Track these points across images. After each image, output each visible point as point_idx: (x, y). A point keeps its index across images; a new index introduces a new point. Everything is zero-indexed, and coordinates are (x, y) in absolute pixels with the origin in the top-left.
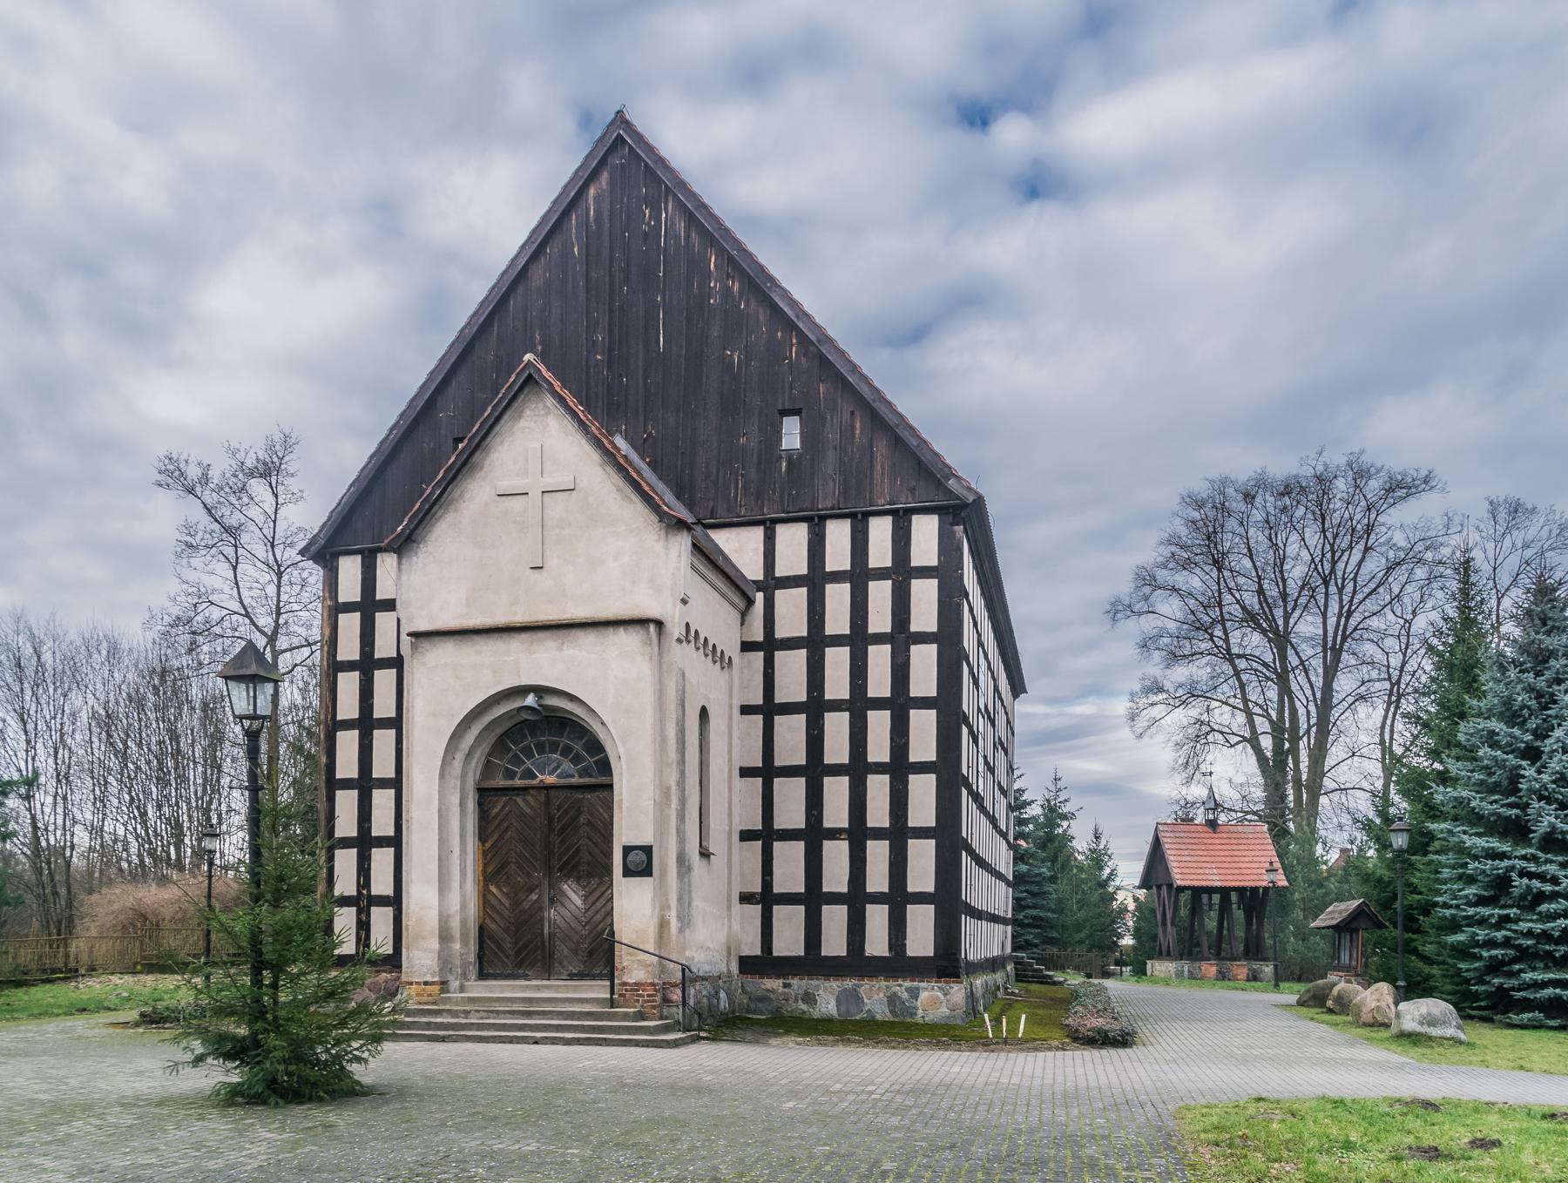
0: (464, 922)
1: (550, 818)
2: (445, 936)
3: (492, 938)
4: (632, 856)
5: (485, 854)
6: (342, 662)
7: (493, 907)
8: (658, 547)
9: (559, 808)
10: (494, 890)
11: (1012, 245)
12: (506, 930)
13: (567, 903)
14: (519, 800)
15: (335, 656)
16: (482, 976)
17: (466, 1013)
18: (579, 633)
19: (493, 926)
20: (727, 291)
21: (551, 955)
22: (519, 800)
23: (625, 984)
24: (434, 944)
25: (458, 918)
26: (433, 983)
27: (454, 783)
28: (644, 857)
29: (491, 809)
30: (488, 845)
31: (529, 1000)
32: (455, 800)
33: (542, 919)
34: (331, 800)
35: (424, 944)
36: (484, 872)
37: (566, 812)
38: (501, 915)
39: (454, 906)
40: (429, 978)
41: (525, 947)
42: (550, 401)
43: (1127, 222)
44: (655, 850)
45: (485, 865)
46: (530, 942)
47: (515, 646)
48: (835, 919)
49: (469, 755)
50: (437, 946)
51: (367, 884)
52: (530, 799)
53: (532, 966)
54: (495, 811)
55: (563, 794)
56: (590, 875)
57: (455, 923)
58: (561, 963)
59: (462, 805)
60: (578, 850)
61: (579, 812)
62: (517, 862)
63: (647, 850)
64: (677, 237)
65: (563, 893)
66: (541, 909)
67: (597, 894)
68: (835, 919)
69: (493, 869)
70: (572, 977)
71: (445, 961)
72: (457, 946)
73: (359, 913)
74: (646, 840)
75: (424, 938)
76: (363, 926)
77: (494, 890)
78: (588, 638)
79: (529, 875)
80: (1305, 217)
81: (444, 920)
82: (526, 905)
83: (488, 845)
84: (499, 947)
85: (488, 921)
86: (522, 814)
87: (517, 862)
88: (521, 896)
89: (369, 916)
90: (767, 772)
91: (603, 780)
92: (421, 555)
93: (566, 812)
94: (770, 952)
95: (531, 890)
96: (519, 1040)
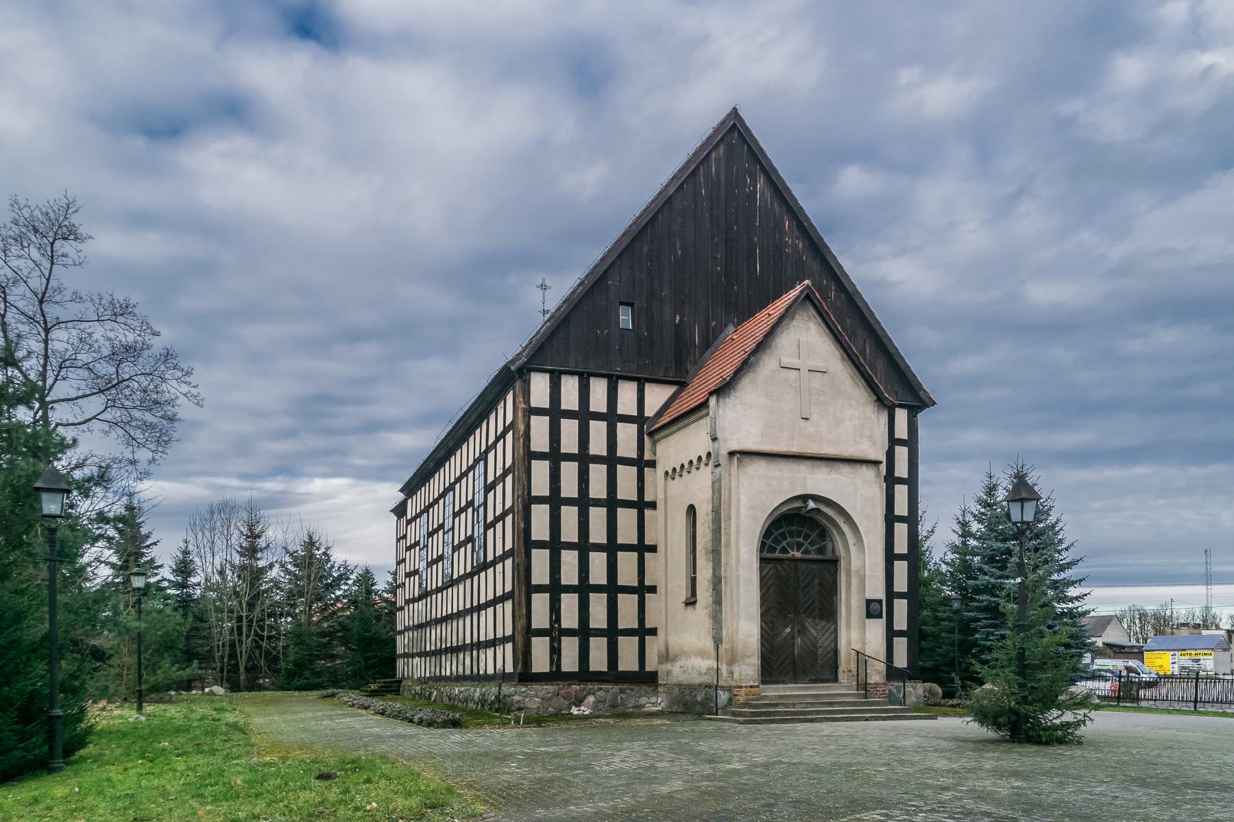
6: (535, 452)
8: (874, 417)
15: (529, 447)
17: (794, 705)
18: (840, 465)
20: (795, 246)
34: (528, 556)
40: (752, 683)
42: (812, 311)
47: (802, 469)
48: (570, 647)
51: (558, 620)
55: (804, 565)
64: (766, 203)
68: (570, 647)
73: (552, 641)
76: (555, 651)
78: (846, 469)
90: (643, 548)
94: (559, 666)
96: (852, 719)
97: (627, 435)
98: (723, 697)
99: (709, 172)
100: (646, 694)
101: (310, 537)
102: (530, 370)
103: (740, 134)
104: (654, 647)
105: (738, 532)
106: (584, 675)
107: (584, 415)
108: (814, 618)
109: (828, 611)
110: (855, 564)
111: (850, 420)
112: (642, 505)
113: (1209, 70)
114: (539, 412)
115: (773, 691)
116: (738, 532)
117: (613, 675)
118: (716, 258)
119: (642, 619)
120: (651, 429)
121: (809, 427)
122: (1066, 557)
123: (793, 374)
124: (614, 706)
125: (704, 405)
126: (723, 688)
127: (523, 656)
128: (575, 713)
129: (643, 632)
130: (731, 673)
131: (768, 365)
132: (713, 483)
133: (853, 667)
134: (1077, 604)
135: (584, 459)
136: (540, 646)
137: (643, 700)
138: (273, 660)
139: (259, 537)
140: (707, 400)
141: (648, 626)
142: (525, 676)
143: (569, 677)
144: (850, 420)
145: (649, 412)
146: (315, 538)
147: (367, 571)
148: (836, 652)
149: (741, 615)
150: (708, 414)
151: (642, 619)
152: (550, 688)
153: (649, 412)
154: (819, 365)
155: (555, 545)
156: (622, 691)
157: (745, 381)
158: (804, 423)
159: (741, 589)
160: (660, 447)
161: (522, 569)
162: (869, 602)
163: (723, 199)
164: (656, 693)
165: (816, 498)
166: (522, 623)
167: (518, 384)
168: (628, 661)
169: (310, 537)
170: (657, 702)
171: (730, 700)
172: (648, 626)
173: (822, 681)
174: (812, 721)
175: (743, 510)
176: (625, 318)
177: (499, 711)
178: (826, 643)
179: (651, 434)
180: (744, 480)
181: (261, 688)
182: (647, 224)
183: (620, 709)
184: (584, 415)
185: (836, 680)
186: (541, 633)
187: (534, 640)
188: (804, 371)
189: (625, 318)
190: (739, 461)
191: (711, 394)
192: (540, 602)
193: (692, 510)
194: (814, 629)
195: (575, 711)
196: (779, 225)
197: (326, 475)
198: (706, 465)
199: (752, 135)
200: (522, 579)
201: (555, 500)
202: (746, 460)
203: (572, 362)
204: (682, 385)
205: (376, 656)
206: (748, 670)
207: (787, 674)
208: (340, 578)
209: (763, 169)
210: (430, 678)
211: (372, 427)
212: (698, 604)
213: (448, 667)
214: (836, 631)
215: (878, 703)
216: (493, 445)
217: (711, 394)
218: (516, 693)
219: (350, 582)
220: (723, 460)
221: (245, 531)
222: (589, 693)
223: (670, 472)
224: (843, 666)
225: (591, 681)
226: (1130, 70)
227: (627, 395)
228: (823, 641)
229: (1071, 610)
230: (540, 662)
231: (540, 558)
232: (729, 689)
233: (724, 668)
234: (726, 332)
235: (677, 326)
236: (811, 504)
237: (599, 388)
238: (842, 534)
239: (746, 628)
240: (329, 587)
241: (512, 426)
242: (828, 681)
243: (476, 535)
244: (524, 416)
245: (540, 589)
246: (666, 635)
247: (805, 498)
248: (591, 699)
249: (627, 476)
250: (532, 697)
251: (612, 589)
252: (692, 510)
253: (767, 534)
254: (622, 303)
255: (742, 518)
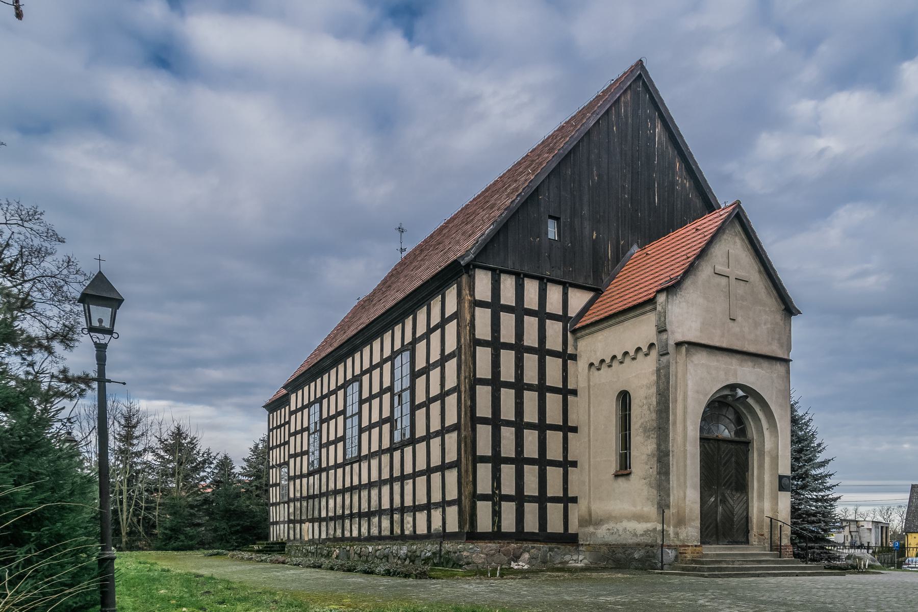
6: (479, 340)
11: (133, 92)
15: (474, 334)
17: (733, 562)
31: (743, 555)
34: (474, 430)
40: (696, 543)
42: (738, 228)
43: (207, 103)
48: (508, 510)
51: (499, 487)
73: (494, 505)
76: (497, 514)
78: (765, 364)
80: (323, 141)
89: (500, 507)
92: (679, 296)
93: (727, 454)
94: (499, 527)
97: (554, 330)
98: (670, 554)
99: (618, 114)
100: (569, 552)
101: (178, 429)
102: (476, 267)
103: (644, 82)
104: (575, 512)
105: (685, 412)
106: (520, 535)
107: (520, 311)
108: (732, 490)
109: (741, 485)
110: (768, 445)
111: (765, 324)
112: (566, 392)
113: (822, 152)
114: (483, 304)
115: (712, 550)
116: (685, 412)
117: (543, 536)
118: (624, 187)
119: (565, 490)
120: (575, 327)
121: (735, 328)
122: (820, 458)
123: (724, 281)
124: (544, 562)
125: (651, 301)
126: (669, 547)
127: (468, 517)
128: (516, 567)
129: (567, 500)
130: (677, 534)
131: (705, 271)
132: (658, 370)
133: (766, 531)
134: (827, 492)
135: (519, 349)
136: (484, 510)
137: (567, 558)
138: (150, 526)
139: (135, 427)
140: (655, 297)
141: (570, 495)
142: (473, 536)
143: (507, 536)
144: (765, 324)
145: (572, 313)
146: (184, 430)
147: (226, 458)
148: (747, 519)
149: (688, 484)
150: (655, 309)
151: (565, 490)
152: (492, 546)
153: (572, 313)
154: (742, 274)
155: (496, 422)
156: (551, 550)
157: (688, 283)
158: (731, 324)
159: (688, 462)
160: (582, 344)
161: (469, 441)
162: (781, 478)
163: (629, 138)
164: (578, 552)
165: (743, 387)
166: (467, 490)
167: (464, 279)
168: (555, 525)
169: (178, 429)
170: (578, 560)
171: (676, 557)
172: (570, 495)
173: (737, 543)
174: (758, 575)
175: (690, 393)
176: (552, 232)
177: (446, 565)
178: (740, 512)
179: (574, 332)
180: (690, 367)
181: (139, 549)
182: (570, 152)
183: (549, 565)
184: (520, 311)
185: (747, 542)
186: (484, 497)
187: (479, 503)
188: (732, 279)
189: (552, 232)
190: (687, 351)
191: (659, 292)
192: (484, 472)
193: (624, 398)
194: (734, 500)
195: (514, 565)
196: (672, 166)
197: (149, 398)
198: (646, 355)
199: (654, 86)
200: (469, 450)
201: (496, 383)
202: (693, 350)
203: (510, 263)
204: (598, 292)
205: (238, 525)
206: (691, 532)
207: (711, 537)
208: (204, 462)
209: (661, 116)
210: (328, 539)
211: (193, 363)
212: (632, 476)
213: (353, 529)
214: (747, 502)
215: (785, 562)
216: (435, 332)
217: (659, 292)
218: (465, 550)
219: (212, 466)
220: (671, 349)
221: (123, 422)
222: (525, 551)
223: (619, 357)
224: (754, 530)
225: (526, 540)
226: (770, 145)
227: (554, 294)
228: (738, 509)
229: (823, 496)
230: (484, 523)
231: (484, 433)
232: (675, 548)
233: (671, 530)
234: (632, 251)
235: (594, 241)
236: (740, 393)
237: (531, 288)
238: (757, 419)
239: (688, 494)
240: (196, 469)
241: (455, 316)
242: (741, 543)
243: (397, 414)
244: (470, 307)
245: (484, 459)
246: (589, 502)
247: (733, 387)
248: (526, 556)
249: (553, 366)
250: (477, 552)
251: (542, 462)
252: (624, 398)
253: (704, 419)
254: (551, 217)
255: (689, 400)
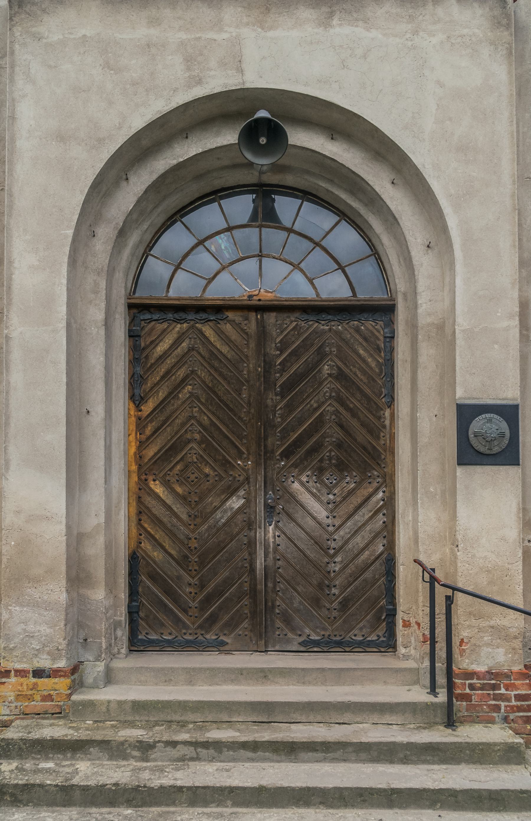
0: (109, 547)
1: (268, 366)
2: (77, 576)
3: (154, 577)
4: (478, 425)
5: (140, 424)
7: (157, 521)
9: (283, 347)
10: (159, 489)
12: (183, 561)
13: (299, 515)
14: (208, 331)
16: (137, 644)
19: (157, 555)
21: (270, 608)
22: (208, 331)
23: (470, 675)
24: (57, 592)
25: (101, 540)
26: (55, 673)
27: (95, 282)
28: (504, 426)
29: (154, 343)
30: (148, 408)
32: (96, 314)
33: (251, 544)
35: (34, 593)
36: (139, 457)
37: (296, 354)
38: (171, 534)
39: (94, 519)
40: (44, 662)
41: (218, 593)
44: (520, 407)
45: (142, 445)
46: (227, 583)
49: (122, 233)
50: (63, 596)
52: (228, 328)
53: (231, 625)
54: (161, 349)
55: (291, 322)
56: (342, 467)
57: (95, 549)
58: (287, 620)
59: (108, 324)
60: (320, 422)
61: (321, 355)
62: (203, 441)
63: (510, 413)
65: (293, 498)
66: (250, 525)
67: (356, 500)
69: (158, 456)
70: (309, 646)
71: (78, 623)
72: (99, 594)
74: (508, 392)
75: (37, 581)
77: (159, 489)
79: (226, 464)
81: (76, 539)
82: (221, 517)
83: (148, 408)
84: (169, 592)
85: (146, 545)
86: (213, 356)
87: (203, 441)
88: (212, 500)
91: (369, 292)
93: (296, 354)
95: (231, 491)
